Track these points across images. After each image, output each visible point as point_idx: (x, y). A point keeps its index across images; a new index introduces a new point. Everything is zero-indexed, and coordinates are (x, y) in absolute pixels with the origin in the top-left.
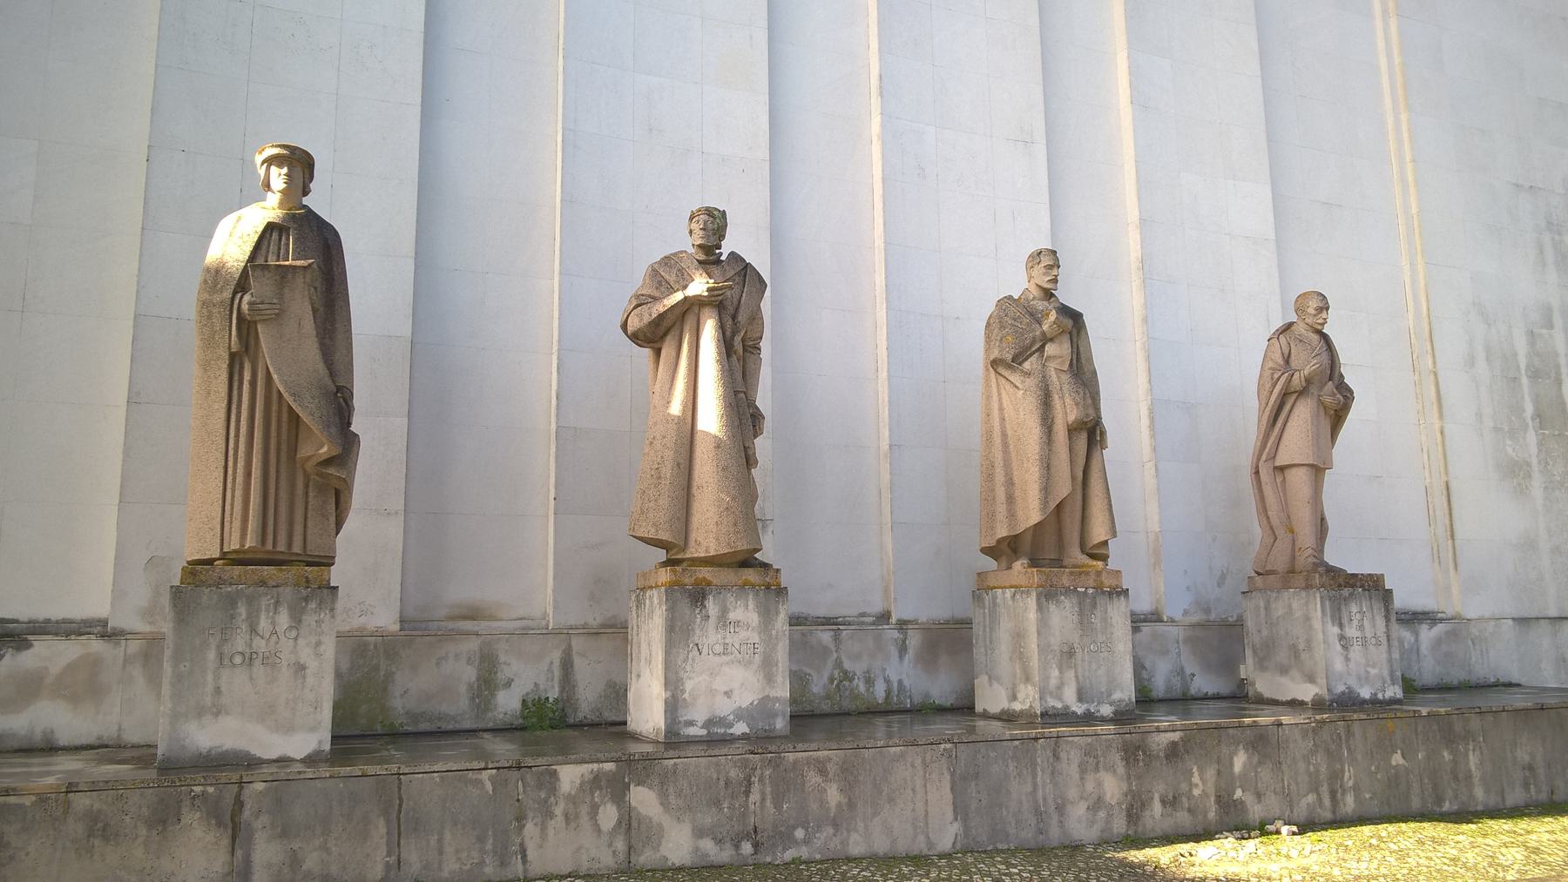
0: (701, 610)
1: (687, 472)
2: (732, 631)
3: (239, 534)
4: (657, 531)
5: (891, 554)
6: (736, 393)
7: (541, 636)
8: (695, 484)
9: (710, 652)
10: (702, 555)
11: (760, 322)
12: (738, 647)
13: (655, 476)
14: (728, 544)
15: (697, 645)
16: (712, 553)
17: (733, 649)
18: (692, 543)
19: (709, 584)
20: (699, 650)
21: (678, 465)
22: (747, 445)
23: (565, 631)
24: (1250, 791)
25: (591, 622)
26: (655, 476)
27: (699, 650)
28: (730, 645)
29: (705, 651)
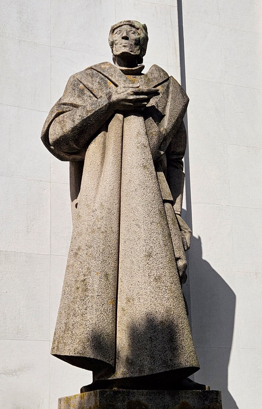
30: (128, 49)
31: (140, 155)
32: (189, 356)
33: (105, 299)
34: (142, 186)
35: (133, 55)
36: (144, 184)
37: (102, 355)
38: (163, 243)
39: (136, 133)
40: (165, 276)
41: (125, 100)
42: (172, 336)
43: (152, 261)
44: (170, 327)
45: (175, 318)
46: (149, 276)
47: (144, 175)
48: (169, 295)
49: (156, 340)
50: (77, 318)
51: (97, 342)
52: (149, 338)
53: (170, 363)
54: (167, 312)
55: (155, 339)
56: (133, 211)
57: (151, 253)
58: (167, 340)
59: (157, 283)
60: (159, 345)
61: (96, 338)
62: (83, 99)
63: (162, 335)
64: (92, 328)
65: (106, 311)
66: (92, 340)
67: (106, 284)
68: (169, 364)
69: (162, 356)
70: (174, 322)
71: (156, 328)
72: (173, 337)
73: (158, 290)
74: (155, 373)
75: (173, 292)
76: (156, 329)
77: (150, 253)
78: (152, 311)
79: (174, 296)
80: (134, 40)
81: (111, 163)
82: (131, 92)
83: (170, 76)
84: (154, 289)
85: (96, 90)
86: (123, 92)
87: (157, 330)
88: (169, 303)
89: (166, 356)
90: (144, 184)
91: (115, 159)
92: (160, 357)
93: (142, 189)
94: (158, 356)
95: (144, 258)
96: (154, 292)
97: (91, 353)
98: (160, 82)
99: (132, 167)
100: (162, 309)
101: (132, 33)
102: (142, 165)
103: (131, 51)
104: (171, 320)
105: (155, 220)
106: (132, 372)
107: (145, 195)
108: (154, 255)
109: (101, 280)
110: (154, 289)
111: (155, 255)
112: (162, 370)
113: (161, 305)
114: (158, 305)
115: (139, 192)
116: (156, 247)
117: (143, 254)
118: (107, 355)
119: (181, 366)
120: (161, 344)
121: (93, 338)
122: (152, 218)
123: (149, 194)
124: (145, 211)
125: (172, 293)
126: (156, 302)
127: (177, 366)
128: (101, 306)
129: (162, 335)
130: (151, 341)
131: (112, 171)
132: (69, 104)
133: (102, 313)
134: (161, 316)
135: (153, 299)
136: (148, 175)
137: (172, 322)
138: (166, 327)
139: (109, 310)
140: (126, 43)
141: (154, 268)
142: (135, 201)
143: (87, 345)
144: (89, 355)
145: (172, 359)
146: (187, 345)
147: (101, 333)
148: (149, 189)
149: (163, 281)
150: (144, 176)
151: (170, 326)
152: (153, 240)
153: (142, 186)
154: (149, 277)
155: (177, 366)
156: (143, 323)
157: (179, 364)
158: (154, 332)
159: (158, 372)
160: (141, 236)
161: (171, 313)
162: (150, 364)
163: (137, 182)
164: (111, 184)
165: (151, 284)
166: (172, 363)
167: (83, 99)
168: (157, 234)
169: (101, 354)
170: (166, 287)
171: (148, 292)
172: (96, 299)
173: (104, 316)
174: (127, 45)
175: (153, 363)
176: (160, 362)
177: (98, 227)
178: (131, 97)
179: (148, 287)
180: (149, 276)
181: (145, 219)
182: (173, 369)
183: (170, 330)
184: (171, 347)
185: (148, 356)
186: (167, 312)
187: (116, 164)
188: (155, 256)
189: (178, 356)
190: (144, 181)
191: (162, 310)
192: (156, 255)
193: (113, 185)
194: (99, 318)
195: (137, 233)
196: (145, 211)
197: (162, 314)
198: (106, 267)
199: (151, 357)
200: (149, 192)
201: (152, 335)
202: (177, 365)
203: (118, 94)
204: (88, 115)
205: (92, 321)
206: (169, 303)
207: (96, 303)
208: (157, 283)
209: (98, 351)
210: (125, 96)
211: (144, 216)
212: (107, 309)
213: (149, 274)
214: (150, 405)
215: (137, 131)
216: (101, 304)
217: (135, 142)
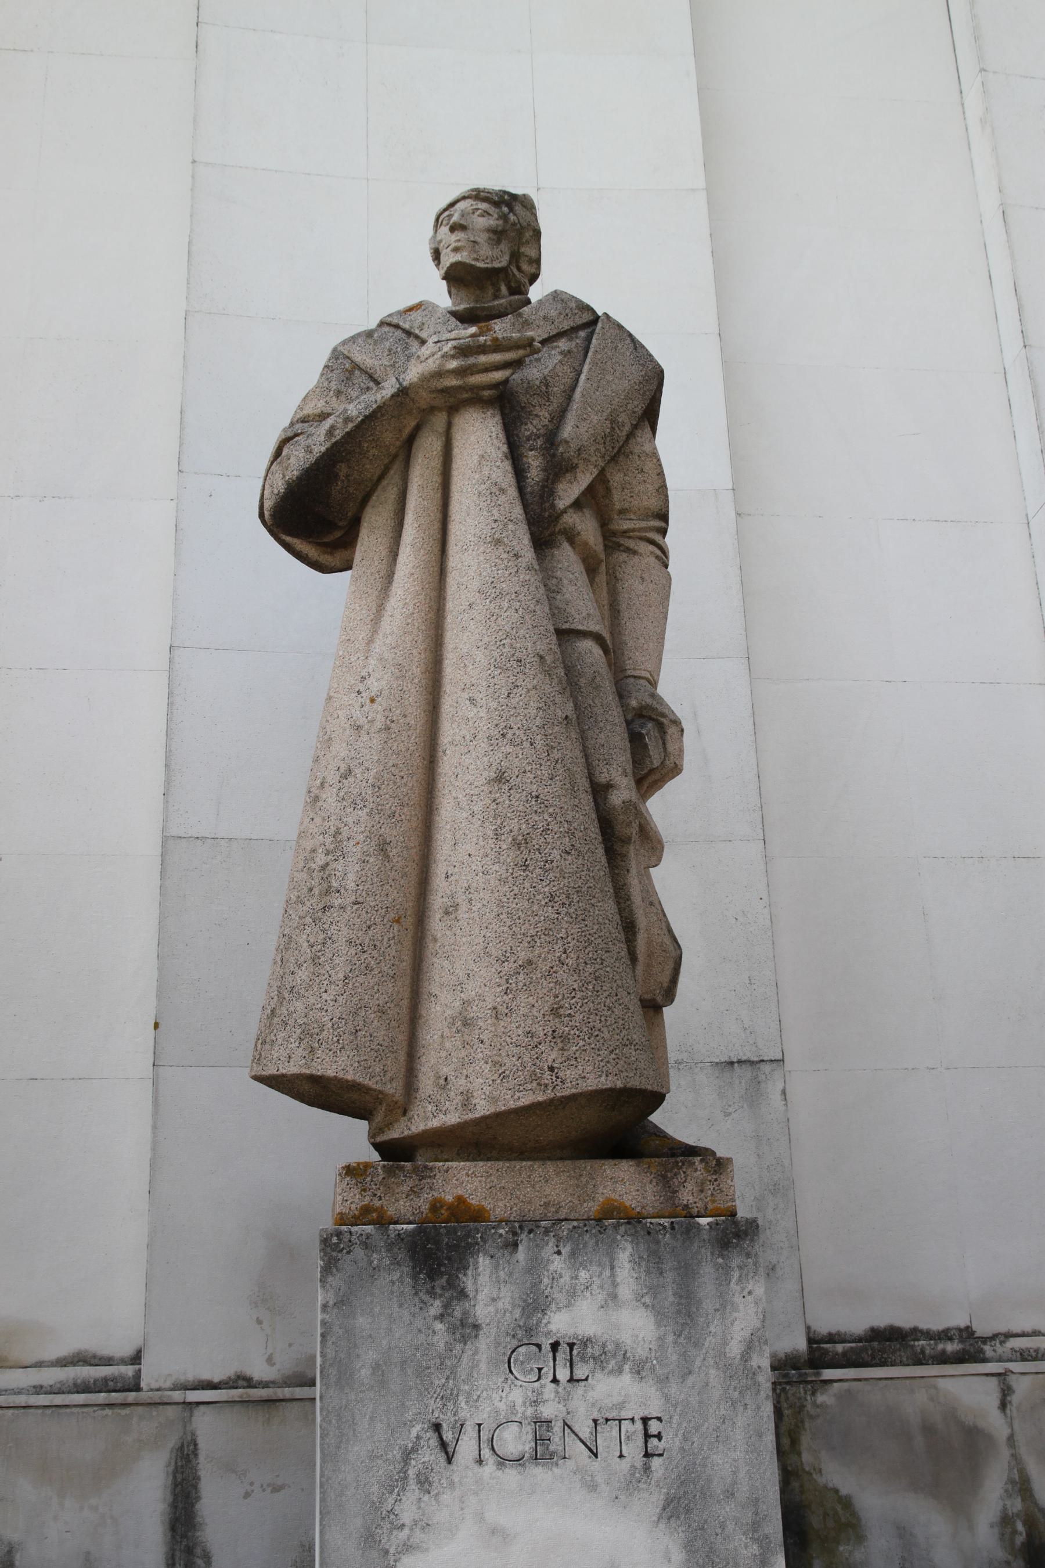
0: (446, 1306)
1: (412, 870)
2: (563, 1374)
3: (778, 1488)
4: (312, 1050)
5: (490, 304)
6: (565, 635)
7: (108, 1412)
8: (438, 901)
9: (486, 1452)
10: (453, 1118)
11: (649, 466)
12: (585, 1431)
13: (316, 891)
14: (534, 1077)
15: (437, 1427)
16: (482, 1108)
17: (570, 1439)
18: (426, 1084)
19: (478, 1215)
20: (443, 1445)
21: (383, 848)
22: (603, 779)
23: (177, 1396)
24: (466, 1314)
25: (259, 1371)
26: (316, 891)
27: (443, 1445)
28: (557, 1426)
29: (466, 1448)
30: (465, 254)
31: (485, 513)
32: (613, 1056)
33: (375, 912)
34: (489, 594)
35: (480, 268)
36: (494, 587)
37: (360, 1066)
38: (542, 742)
39: (477, 457)
40: (544, 833)
41: (439, 374)
42: (560, 1001)
43: (509, 794)
44: (554, 974)
45: (570, 950)
46: (496, 834)
47: (493, 564)
48: (556, 883)
49: (509, 1014)
50: (303, 968)
51: (346, 1032)
52: (490, 1009)
53: (549, 1077)
54: (546, 933)
55: (506, 1011)
56: (462, 665)
57: (504, 772)
58: (542, 1012)
59: (519, 853)
60: (517, 1028)
61: (343, 1021)
62: (349, 397)
63: (528, 998)
64: (335, 993)
65: (378, 943)
66: (332, 1027)
67: (382, 869)
68: (547, 1082)
69: (526, 1059)
70: (567, 961)
71: (510, 981)
72: (562, 1003)
73: (522, 873)
74: (503, 1108)
75: (566, 875)
76: (511, 984)
77: (503, 771)
78: (501, 934)
79: (574, 888)
80: (483, 231)
81: (409, 546)
82: (451, 349)
83: (600, 314)
84: (510, 871)
85: (382, 368)
86: (433, 355)
87: (514, 985)
88: (553, 907)
89: (537, 1058)
90: (494, 587)
91: (422, 535)
92: (520, 1061)
93: (488, 601)
94: (514, 1059)
95: (485, 788)
96: (510, 878)
97: (327, 1062)
98: (563, 328)
99: (464, 548)
100: (531, 925)
101: (479, 216)
102: (489, 539)
103: (477, 260)
104: (559, 954)
105: (522, 680)
106: (446, 1111)
107: (495, 617)
108: (514, 778)
109: (367, 858)
110: (510, 871)
111: (517, 776)
112: (523, 1100)
113: (528, 913)
114: (520, 914)
115: (479, 611)
116: (520, 755)
117: (483, 777)
118: (375, 1065)
119: (585, 1084)
120: (523, 1025)
121: (334, 1019)
122: (512, 678)
123: (508, 613)
124: (493, 660)
125: (564, 878)
126: (514, 906)
127: (569, 1085)
128: (364, 930)
129: (528, 998)
130: (497, 1018)
131: (411, 565)
132: (315, 415)
133: (365, 949)
134: (526, 944)
135: (506, 900)
136: (506, 562)
137: (559, 961)
138: (540, 975)
139: (386, 939)
140: (459, 241)
141: (513, 812)
142: (468, 636)
143: (320, 1040)
144: (324, 1067)
145: (555, 1065)
146: (611, 1025)
147: (359, 1006)
148: (506, 600)
149: (537, 846)
150: (496, 565)
151: (554, 972)
152: (514, 734)
153: (489, 594)
154: (497, 839)
155: (569, 1085)
156: (475, 969)
157: (577, 1080)
158: (506, 993)
159: (513, 1106)
160: (479, 729)
161: (558, 936)
162: (491, 1083)
163: (476, 584)
164: (407, 601)
165: (501, 858)
166: (554, 1078)
167: (349, 397)
168: (527, 718)
169: (356, 1064)
170: (547, 862)
171: (492, 882)
172: (349, 913)
173: (370, 959)
174: (463, 244)
175: (499, 1081)
176: (519, 1076)
177: (369, 718)
178: (453, 364)
179: (491, 866)
180: (496, 834)
181: (491, 680)
182: (558, 1094)
183: (552, 985)
184: (554, 1031)
185: (487, 1063)
186: (546, 933)
187: (425, 546)
188: (519, 779)
189: (576, 1058)
190: (493, 580)
191: (532, 927)
192: (520, 776)
193: (414, 602)
194: (355, 964)
195: (471, 722)
196: (494, 659)
197: (529, 939)
198: (382, 822)
199: (495, 1063)
200: (505, 609)
201: (498, 999)
202: (571, 1082)
203: (421, 362)
204: (347, 430)
205: (337, 973)
206: (553, 907)
207: (350, 926)
208: (519, 853)
209: (348, 1056)
210: (437, 362)
211: (489, 672)
212: (380, 938)
213: (496, 829)
214: (501, 1204)
215: (480, 453)
216: (364, 925)
217: (474, 481)
